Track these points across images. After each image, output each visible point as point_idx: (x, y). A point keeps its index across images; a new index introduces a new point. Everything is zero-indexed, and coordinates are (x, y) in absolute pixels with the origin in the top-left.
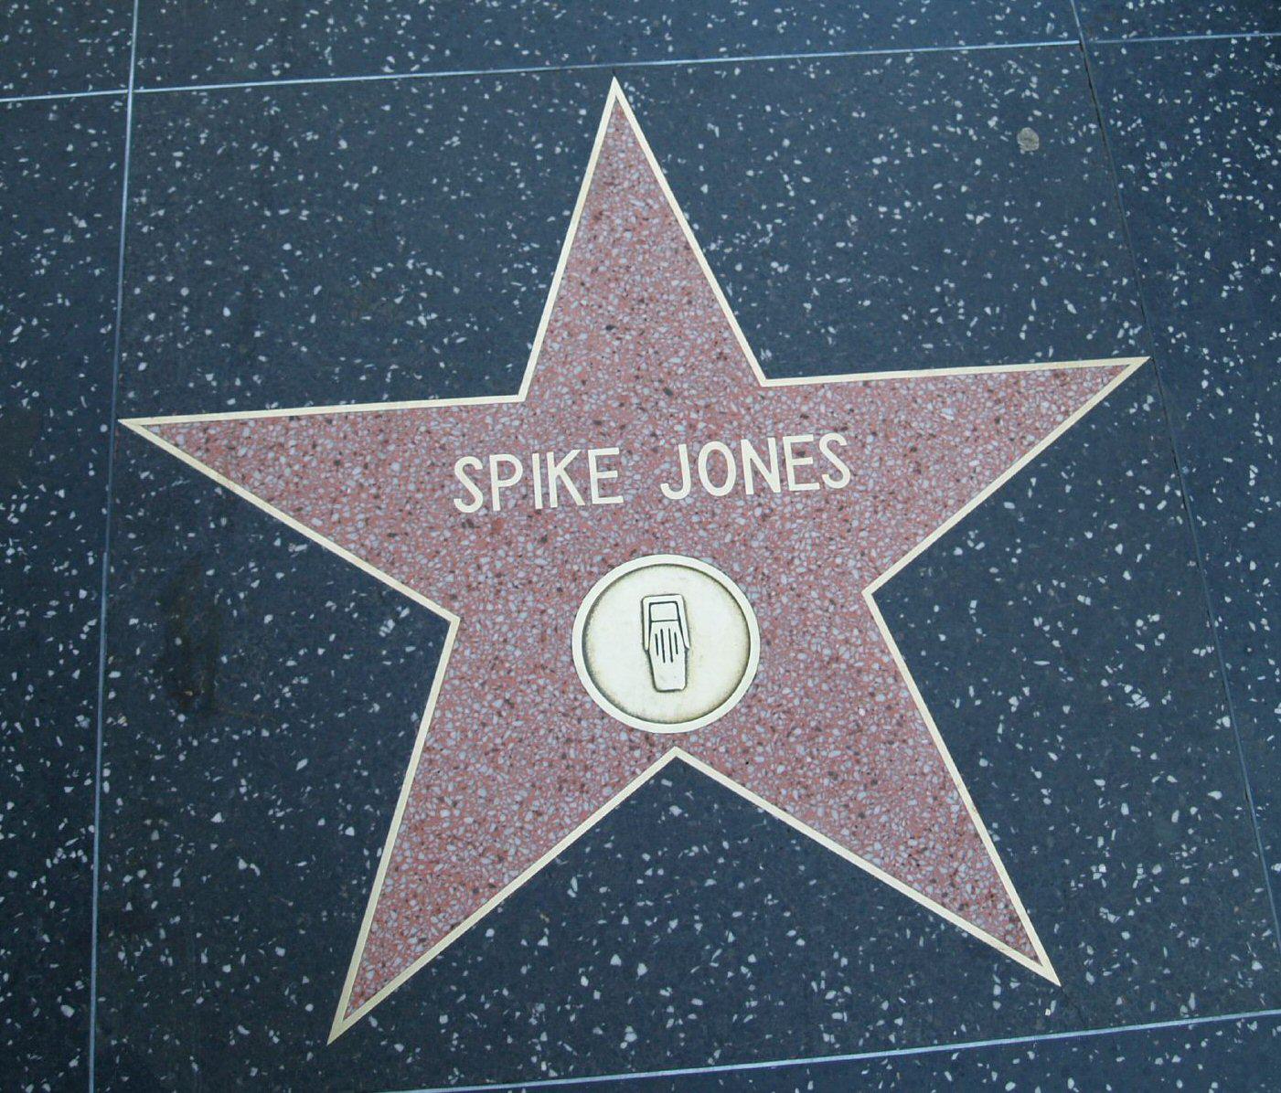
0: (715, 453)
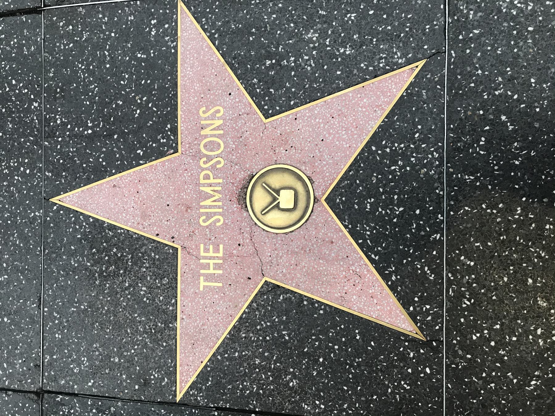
0: (205, 146)
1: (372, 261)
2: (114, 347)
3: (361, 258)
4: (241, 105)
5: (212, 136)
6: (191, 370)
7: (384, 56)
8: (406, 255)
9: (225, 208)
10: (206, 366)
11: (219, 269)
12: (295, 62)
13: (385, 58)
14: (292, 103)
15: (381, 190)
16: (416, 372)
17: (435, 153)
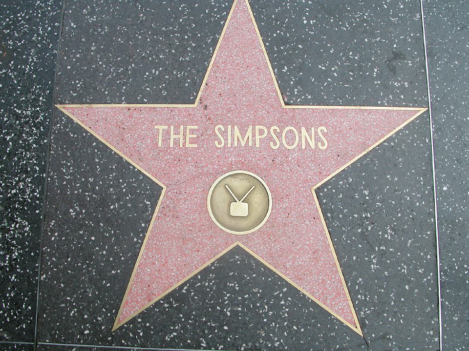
0: (291, 131)
1: (181, 287)
2: (105, 46)
3: (184, 277)
4: (328, 166)
5: (300, 138)
6: (83, 117)
7: (368, 299)
8: (187, 316)
9: (232, 150)
10: (87, 132)
11: (175, 143)
12: (366, 217)
13: (366, 300)
14: (329, 215)
15: (246, 296)
16: (85, 322)
17: (278, 343)
